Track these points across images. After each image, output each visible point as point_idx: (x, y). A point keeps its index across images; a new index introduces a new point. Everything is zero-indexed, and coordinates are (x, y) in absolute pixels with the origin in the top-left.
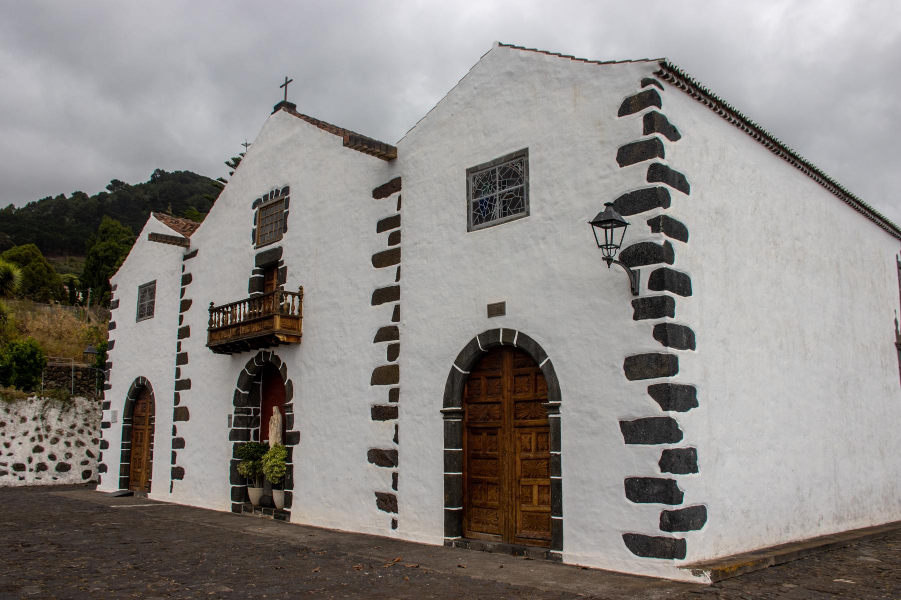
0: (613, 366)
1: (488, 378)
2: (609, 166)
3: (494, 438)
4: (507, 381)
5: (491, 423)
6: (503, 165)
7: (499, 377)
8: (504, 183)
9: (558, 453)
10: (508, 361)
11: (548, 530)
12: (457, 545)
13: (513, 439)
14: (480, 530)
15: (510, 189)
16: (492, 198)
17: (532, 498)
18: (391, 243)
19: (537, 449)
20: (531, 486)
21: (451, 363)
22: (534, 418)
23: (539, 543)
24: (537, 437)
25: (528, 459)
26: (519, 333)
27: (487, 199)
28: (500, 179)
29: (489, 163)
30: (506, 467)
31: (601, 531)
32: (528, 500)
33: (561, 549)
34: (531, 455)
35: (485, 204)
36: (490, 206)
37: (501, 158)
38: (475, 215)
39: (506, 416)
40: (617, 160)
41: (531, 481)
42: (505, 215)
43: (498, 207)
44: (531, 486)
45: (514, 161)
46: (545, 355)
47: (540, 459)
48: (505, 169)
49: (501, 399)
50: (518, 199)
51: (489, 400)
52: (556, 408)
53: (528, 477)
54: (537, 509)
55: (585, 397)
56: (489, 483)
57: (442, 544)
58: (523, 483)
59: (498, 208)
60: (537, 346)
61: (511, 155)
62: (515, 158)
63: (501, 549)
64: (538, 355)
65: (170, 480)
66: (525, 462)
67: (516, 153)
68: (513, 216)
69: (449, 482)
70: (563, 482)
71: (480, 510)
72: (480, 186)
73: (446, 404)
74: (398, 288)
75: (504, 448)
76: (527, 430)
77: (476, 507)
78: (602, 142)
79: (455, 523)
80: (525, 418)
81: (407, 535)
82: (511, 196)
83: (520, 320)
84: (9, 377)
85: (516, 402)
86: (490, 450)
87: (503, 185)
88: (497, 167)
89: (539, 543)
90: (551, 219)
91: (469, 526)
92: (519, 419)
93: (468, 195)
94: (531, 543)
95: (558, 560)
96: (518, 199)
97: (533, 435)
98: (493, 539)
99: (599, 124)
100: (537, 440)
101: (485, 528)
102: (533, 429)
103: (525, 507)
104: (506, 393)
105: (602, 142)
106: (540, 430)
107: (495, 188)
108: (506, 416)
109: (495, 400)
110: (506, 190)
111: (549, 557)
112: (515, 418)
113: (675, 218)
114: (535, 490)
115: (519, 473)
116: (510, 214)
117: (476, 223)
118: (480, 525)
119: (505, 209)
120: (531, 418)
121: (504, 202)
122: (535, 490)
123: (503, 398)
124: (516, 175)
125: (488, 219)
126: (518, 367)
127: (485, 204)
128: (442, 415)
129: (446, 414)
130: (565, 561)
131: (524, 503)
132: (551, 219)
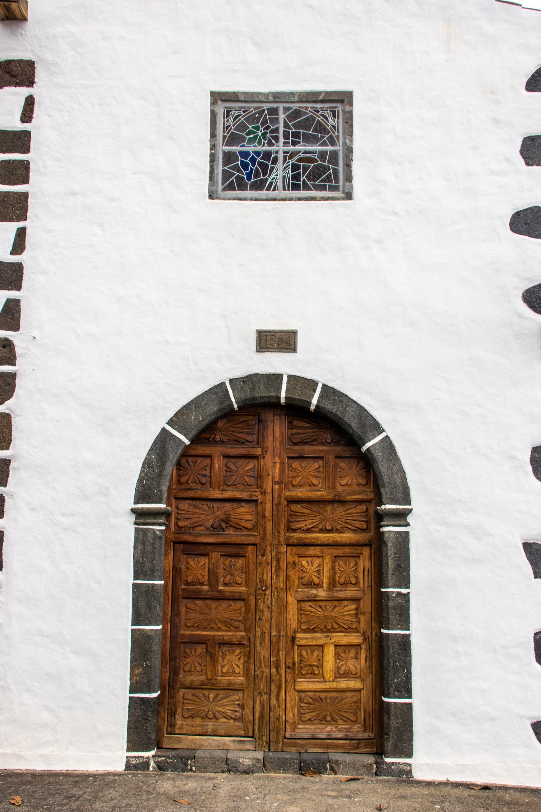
0: (513, 458)
1: (227, 456)
2: (508, 160)
3: (240, 562)
4: (272, 464)
5: (231, 536)
6: (295, 106)
7: (256, 457)
8: (296, 135)
9: (404, 591)
10: (276, 429)
11: (355, 722)
12: (161, 767)
13: (283, 566)
14: (198, 730)
15: (309, 148)
16: (267, 155)
17: (321, 666)
19: (333, 584)
20: (322, 646)
21: (160, 422)
22: (329, 531)
23: (337, 746)
24: (333, 562)
25: (314, 599)
26: (324, 386)
27: (258, 153)
28: (286, 125)
29: (266, 95)
30: (267, 614)
31: (492, 719)
32: (314, 671)
33: (410, 755)
34: (322, 594)
35: (253, 160)
36: (264, 168)
37: (292, 94)
38: (226, 175)
39: (269, 525)
40: (521, 153)
41: (319, 638)
42: (295, 187)
43: (280, 172)
44: (322, 646)
45: (319, 106)
46: (378, 428)
47: (340, 600)
48: (297, 113)
49: (257, 494)
50: (327, 169)
51: (229, 495)
52: (401, 517)
53: (314, 631)
54: (334, 685)
55: (460, 501)
56: (222, 643)
57: (120, 767)
58: (303, 642)
59: (281, 174)
60: (362, 412)
61: (316, 94)
62: (322, 101)
63: (265, 765)
64: (363, 426)
66: (306, 606)
67: (327, 93)
68: (314, 193)
69: (140, 645)
70: (413, 639)
71: (199, 693)
72: (242, 127)
73: (140, 497)
74: (18, 269)
75: (262, 581)
76: (312, 551)
77: (191, 687)
78: (497, 121)
79: (147, 725)
80: (308, 531)
81: (19, 757)
82: (312, 160)
83: (319, 362)
84: (178, 675)
85: (292, 502)
86: (226, 585)
87: (293, 138)
88: (281, 106)
89: (337, 746)
90: (396, 214)
91: (172, 725)
92: (294, 531)
93: (213, 135)
94: (321, 746)
95: (404, 775)
96: (327, 169)
97: (328, 560)
98: (232, 746)
99: (492, 93)
100: (333, 568)
101: (210, 726)
102: (325, 549)
103: (303, 684)
104: (268, 485)
105: (497, 121)
106: (340, 551)
107: (277, 139)
108: (269, 525)
109: (245, 495)
110: (297, 148)
111: (380, 770)
112: (290, 529)
113: (4, 303)
114: (330, 653)
115: (293, 624)
116: (306, 188)
117: (230, 187)
118: (198, 721)
119: (296, 177)
120: (322, 531)
121: (295, 167)
122: (330, 653)
123: (264, 493)
124: (321, 128)
125: (259, 186)
126: (295, 444)
127: (253, 160)
128: (133, 518)
129: (140, 515)
130: (418, 775)
131: (303, 676)
132: (396, 214)
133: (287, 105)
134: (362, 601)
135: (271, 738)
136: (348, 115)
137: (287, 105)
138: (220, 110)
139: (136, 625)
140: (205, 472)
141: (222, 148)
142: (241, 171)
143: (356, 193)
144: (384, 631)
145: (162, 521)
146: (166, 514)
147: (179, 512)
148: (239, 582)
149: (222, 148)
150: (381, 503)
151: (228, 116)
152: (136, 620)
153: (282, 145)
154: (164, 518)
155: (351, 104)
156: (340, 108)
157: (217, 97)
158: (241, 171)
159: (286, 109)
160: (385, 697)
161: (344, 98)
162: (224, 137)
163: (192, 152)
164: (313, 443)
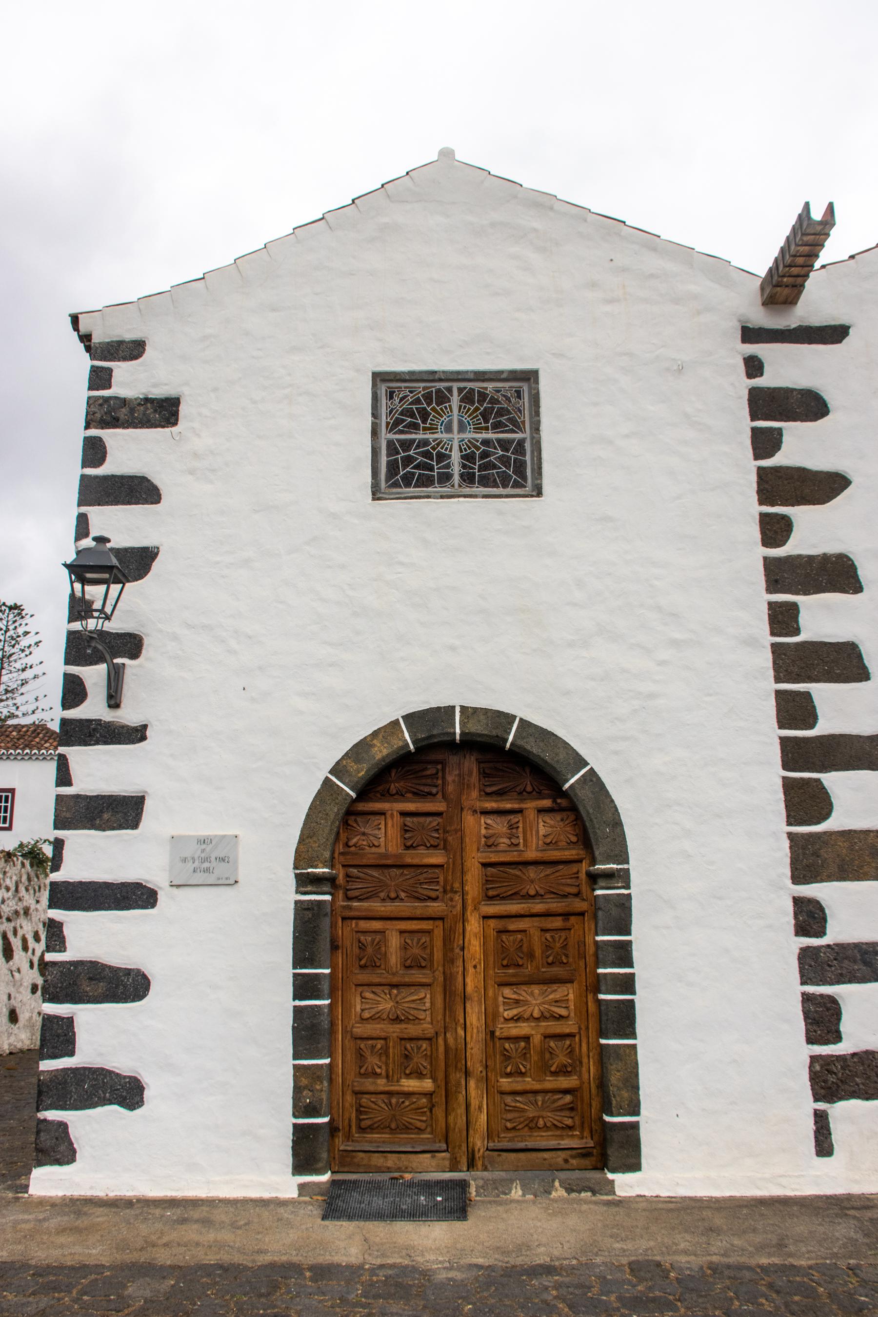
18: (793, 610)
38: (393, 468)
65: (809, 1105)
117: (396, 485)
133: (462, 385)
134: (572, 931)
135: (462, 1011)
136: (533, 392)
137: (462, 385)
138: (383, 389)
139: (301, 999)
140: (376, 832)
141: (385, 436)
142: (407, 465)
143: (546, 488)
144: (603, 1041)
145: (325, 889)
146: (331, 880)
147: (362, 1109)
148: (423, 965)
149: (385, 436)
150: (593, 862)
151: (391, 398)
152: (298, 962)
153: (457, 435)
154: (329, 884)
155: (537, 382)
156: (525, 387)
157: (379, 377)
158: (407, 465)
159: (460, 390)
160: (607, 1115)
161: (530, 377)
162: (388, 424)
163: (350, 439)
164: (513, 897)
